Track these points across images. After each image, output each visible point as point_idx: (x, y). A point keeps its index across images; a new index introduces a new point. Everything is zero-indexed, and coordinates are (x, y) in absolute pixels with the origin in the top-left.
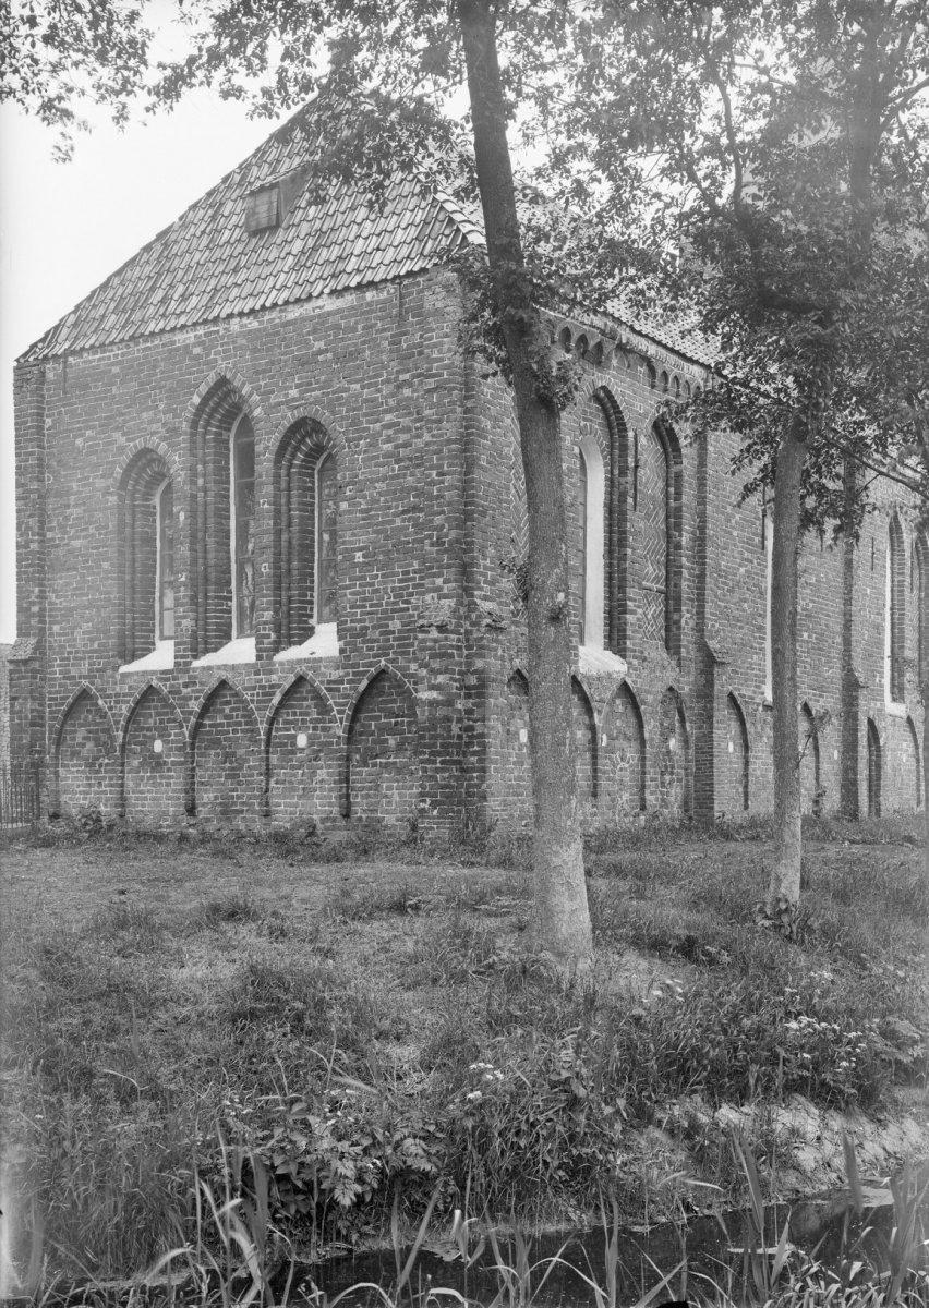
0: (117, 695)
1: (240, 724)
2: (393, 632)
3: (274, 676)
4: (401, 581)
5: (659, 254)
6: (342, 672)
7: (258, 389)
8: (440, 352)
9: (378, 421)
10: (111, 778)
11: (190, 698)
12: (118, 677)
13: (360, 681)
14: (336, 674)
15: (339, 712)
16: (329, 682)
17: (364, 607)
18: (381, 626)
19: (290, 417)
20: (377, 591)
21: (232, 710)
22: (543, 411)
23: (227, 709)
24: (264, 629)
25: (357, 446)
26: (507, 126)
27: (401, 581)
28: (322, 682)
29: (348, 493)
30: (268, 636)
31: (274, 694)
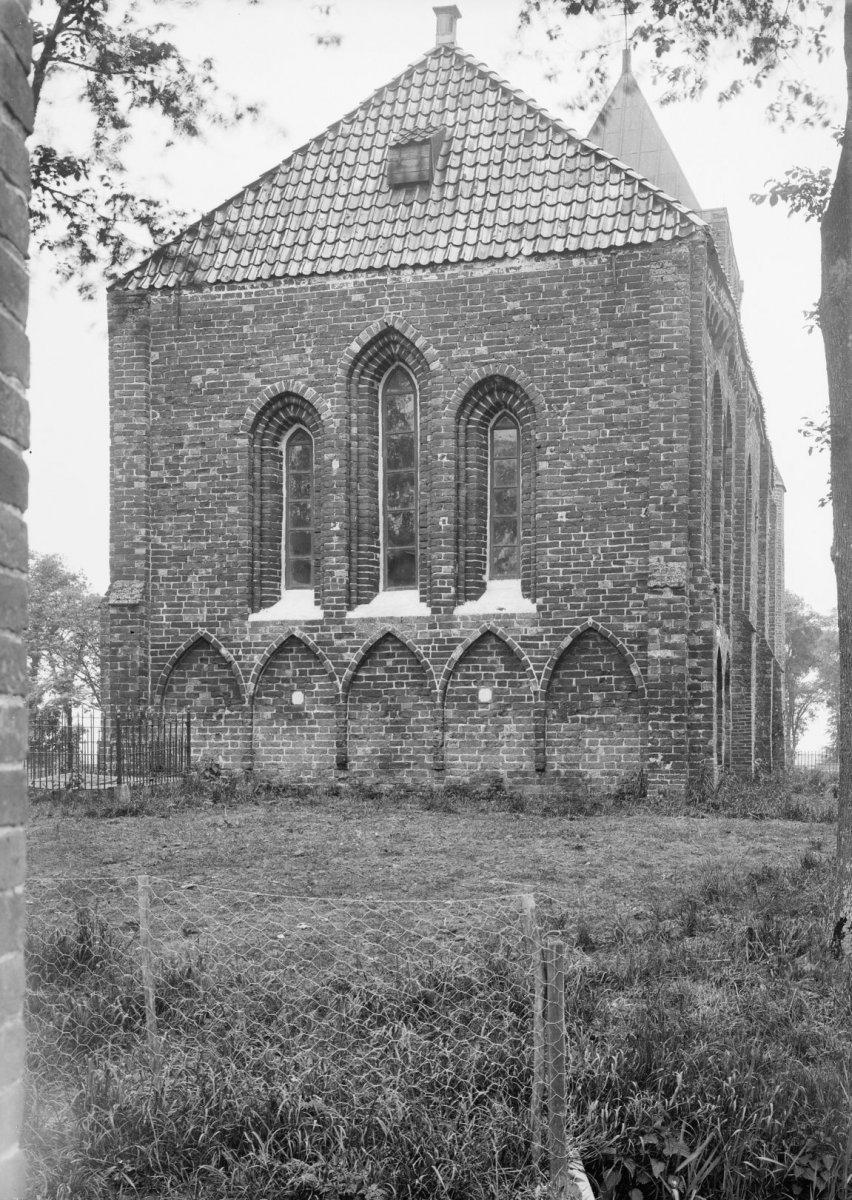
31: (454, 648)
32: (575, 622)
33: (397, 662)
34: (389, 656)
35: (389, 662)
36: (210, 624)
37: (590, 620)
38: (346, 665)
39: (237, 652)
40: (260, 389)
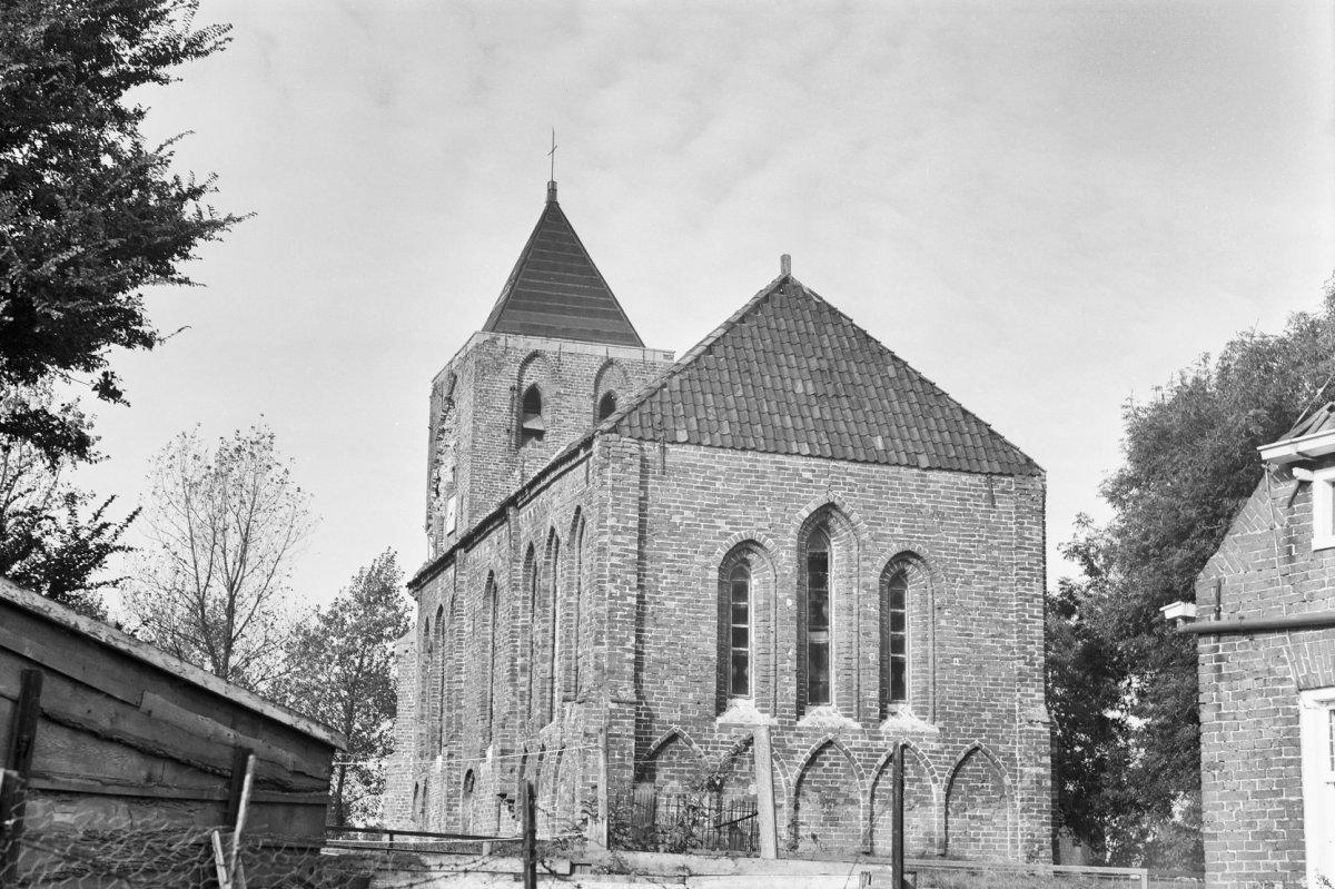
0: (714, 742)
1: (839, 777)
2: (985, 721)
3: (880, 742)
4: (991, 684)
5: (1139, 515)
6: (943, 745)
7: (865, 519)
8: (1031, 533)
9: (972, 567)
10: (836, 770)
11: (796, 752)
12: (717, 727)
13: (958, 753)
14: (936, 746)
15: (940, 775)
16: (931, 752)
17: (961, 698)
18: (976, 715)
19: (895, 549)
20: (972, 689)
21: (831, 765)
22: (46, 711)
23: (826, 764)
24: (871, 705)
25: (954, 581)
26: (138, 168)
27: (991, 684)
28: (925, 751)
29: (946, 614)
30: (875, 711)
31: (880, 756)
32: (967, 742)
33: (831, 765)
34: (825, 759)
35: (826, 764)
36: (683, 722)
37: (977, 742)
38: (797, 764)
39: (707, 748)
40: (729, 534)
